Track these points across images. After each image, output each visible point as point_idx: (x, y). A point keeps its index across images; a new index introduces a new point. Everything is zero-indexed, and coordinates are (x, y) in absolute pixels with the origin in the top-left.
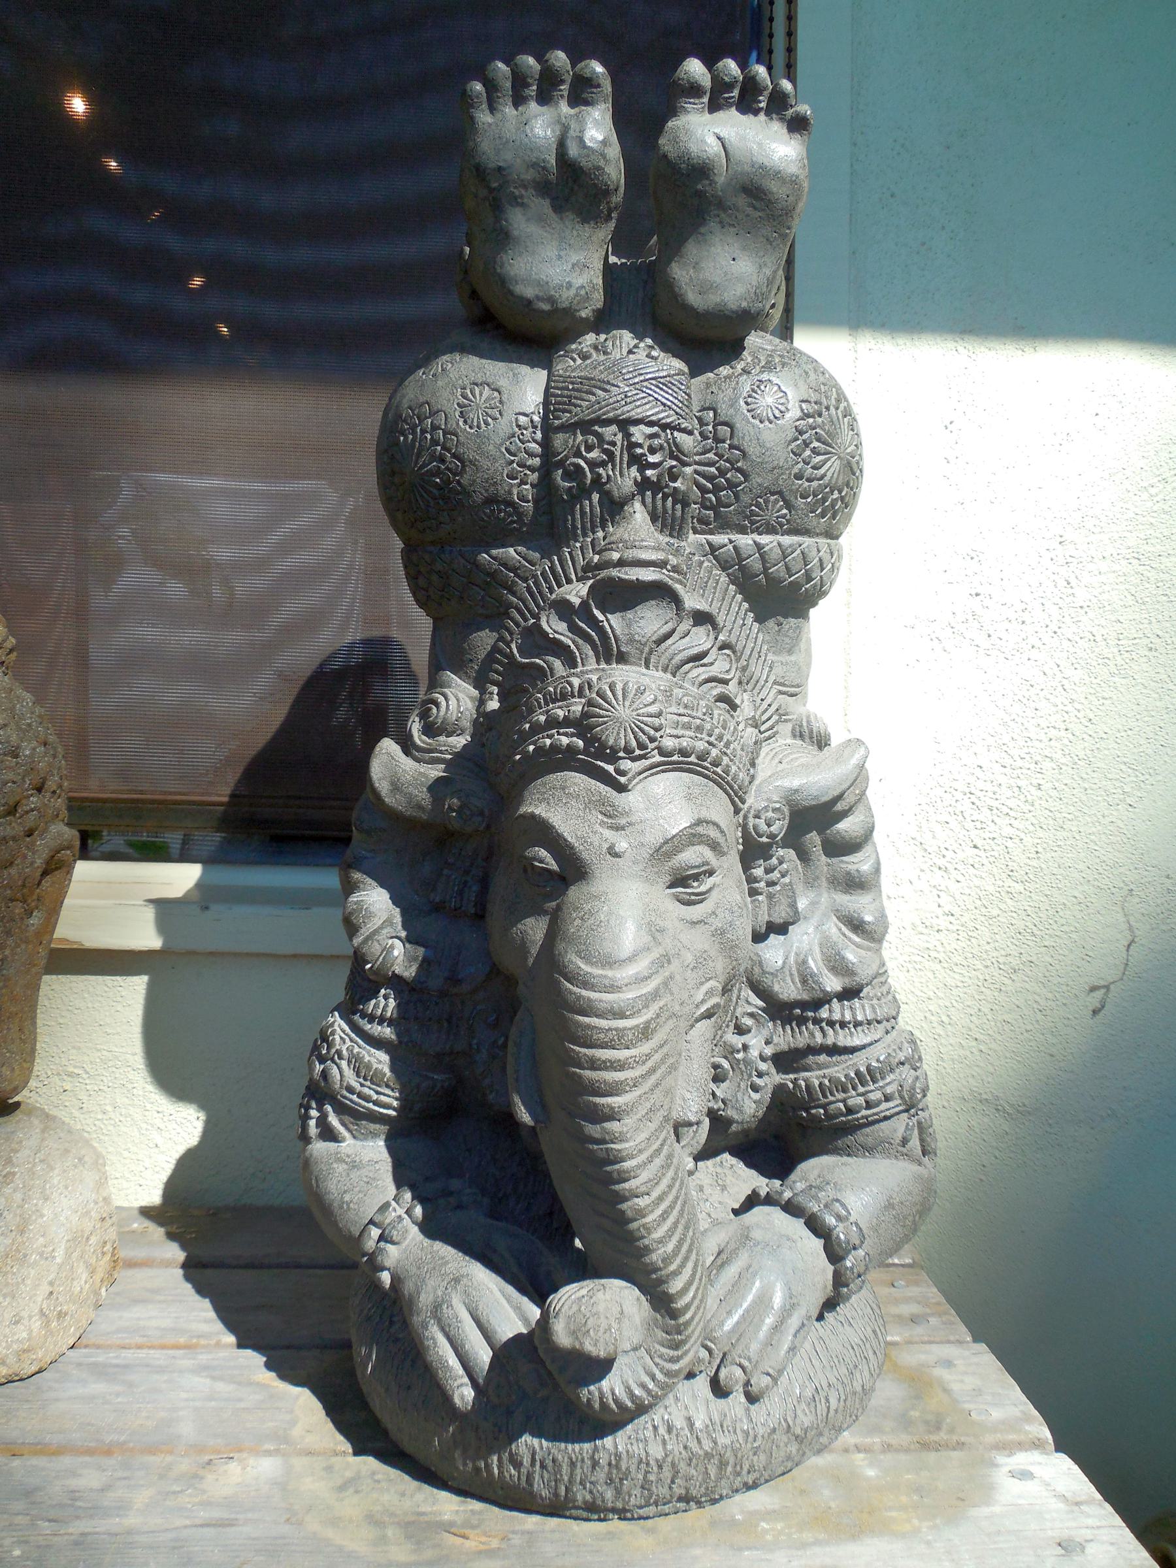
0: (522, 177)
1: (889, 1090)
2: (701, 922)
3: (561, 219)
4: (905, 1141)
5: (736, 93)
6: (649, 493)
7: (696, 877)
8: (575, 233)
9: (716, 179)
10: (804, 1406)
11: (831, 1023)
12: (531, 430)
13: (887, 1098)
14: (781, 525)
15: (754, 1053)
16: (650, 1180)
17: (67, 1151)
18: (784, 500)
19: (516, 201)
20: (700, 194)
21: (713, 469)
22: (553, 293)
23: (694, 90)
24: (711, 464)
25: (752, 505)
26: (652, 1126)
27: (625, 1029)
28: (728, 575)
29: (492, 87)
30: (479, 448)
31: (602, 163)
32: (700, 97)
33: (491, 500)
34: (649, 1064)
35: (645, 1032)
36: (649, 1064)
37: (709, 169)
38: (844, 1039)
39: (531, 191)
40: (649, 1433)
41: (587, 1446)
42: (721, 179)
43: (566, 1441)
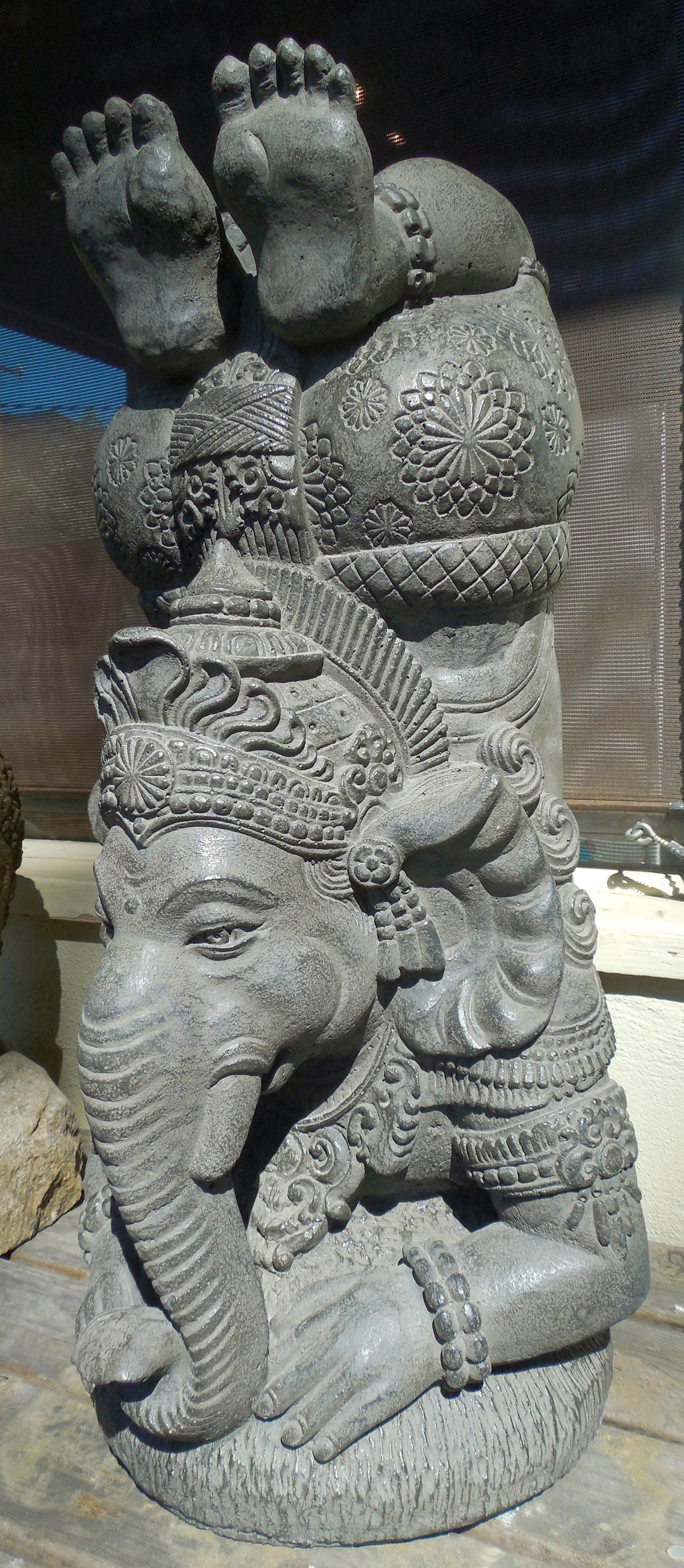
0: (105, 233)
1: (545, 1163)
2: (232, 977)
3: (151, 262)
4: (571, 1225)
5: (272, 77)
6: (256, 523)
7: (216, 933)
8: (168, 271)
9: (261, 180)
10: (386, 1481)
11: (486, 1083)
12: (162, 475)
13: (543, 1173)
14: (406, 534)
15: (399, 1102)
16: (152, 1227)
17: (12, 1099)
18: (399, 507)
19: (110, 257)
20: (253, 200)
21: (321, 486)
22: (157, 336)
23: (231, 91)
24: (319, 481)
25: (364, 518)
26: (153, 1175)
27: (104, 1082)
28: (357, 595)
29: (72, 154)
30: (122, 501)
31: (164, 199)
32: (238, 95)
33: (144, 548)
34: (137, 1117)
35: (125, 1088)
36: (137, 1117)
37: (249, 173)
38: (498, 1099)
39: (118, 244)
40: (213, 1460)
41: (165, 1455)
42: (266, 179)
43: (151, 1447)
